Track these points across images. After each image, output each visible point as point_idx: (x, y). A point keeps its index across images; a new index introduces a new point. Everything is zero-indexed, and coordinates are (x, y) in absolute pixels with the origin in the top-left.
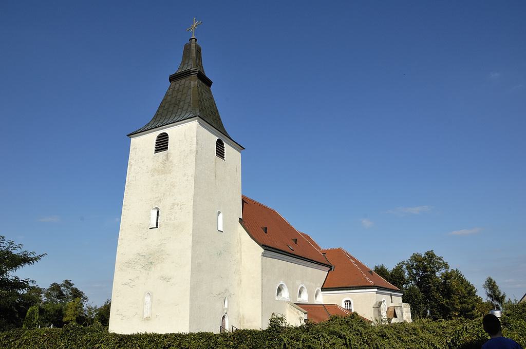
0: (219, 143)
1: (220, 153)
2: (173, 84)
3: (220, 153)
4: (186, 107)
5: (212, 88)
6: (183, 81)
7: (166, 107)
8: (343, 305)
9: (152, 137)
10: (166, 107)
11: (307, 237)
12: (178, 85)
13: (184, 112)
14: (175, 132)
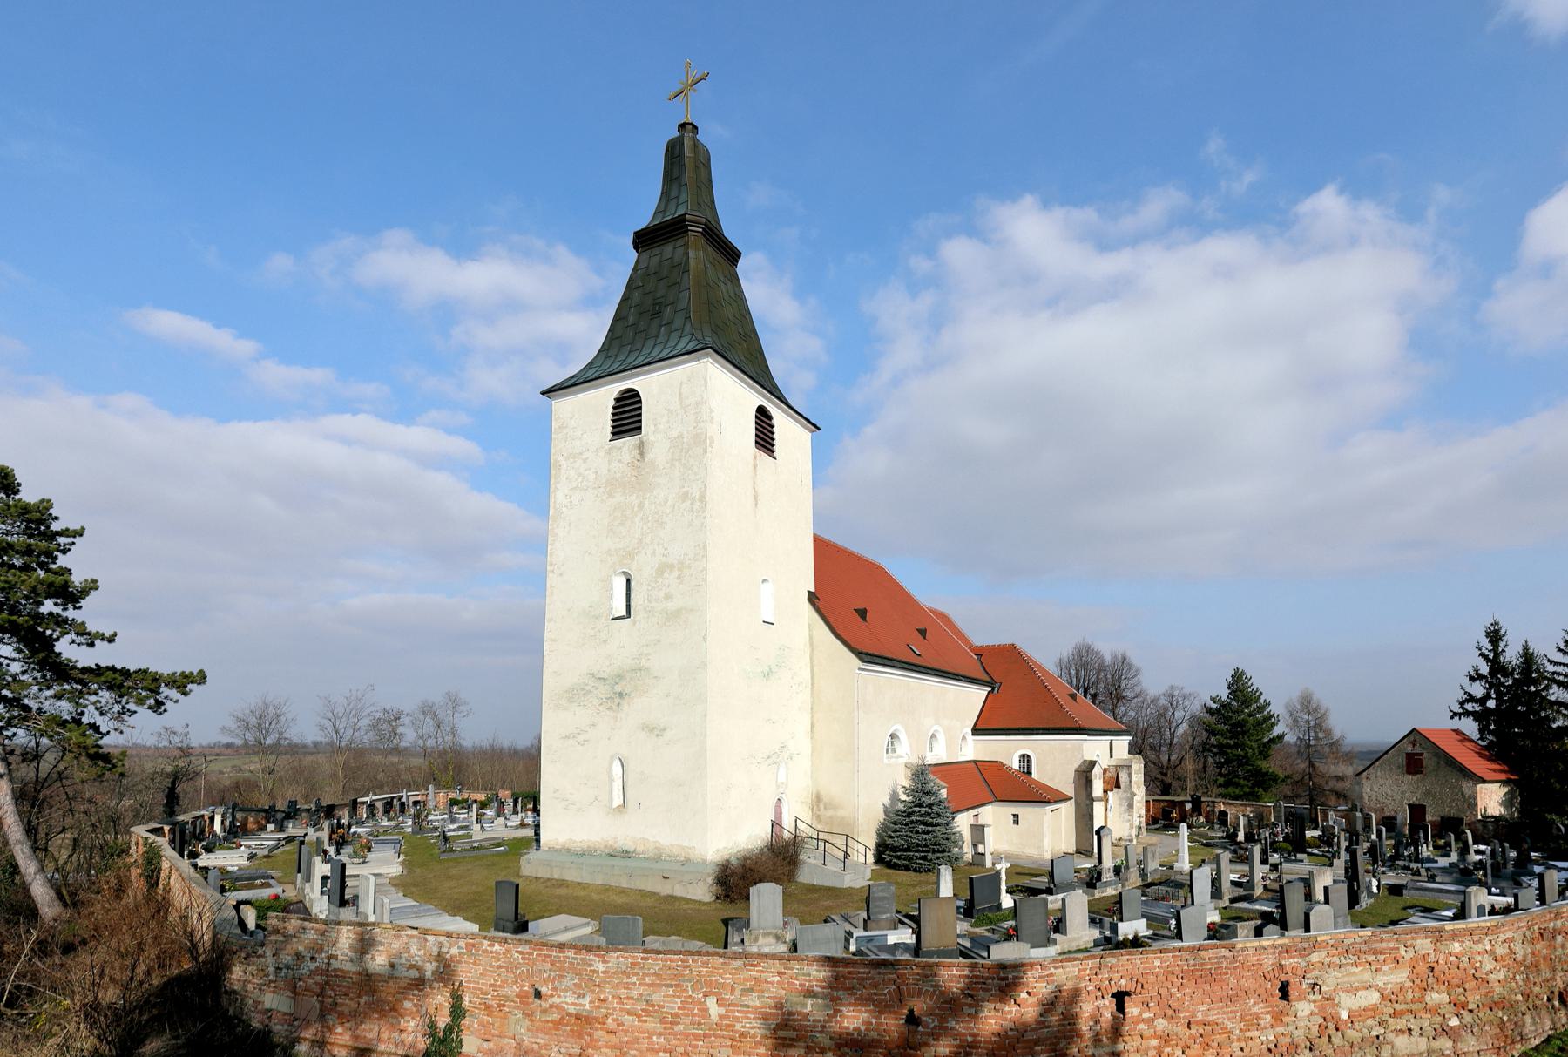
0: (762, 412)
1: (765, 439)
2: (645, 256)
3: (765, 439)
4: (678, 323)
5: (742, 266)
6: (668, 250)
7: (631, 319)
8: (1016, 765)
9: (605, 396)
10: (631, 319)
11: (944, 618)
12: (656, 260)
13: (675, 336)
14: (652, 385)
